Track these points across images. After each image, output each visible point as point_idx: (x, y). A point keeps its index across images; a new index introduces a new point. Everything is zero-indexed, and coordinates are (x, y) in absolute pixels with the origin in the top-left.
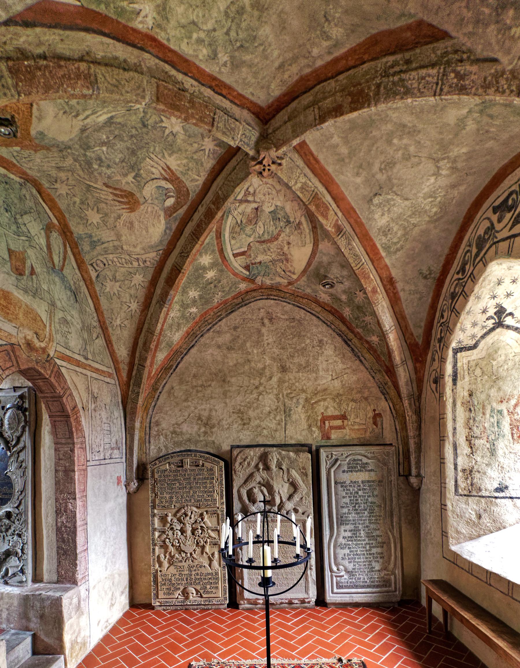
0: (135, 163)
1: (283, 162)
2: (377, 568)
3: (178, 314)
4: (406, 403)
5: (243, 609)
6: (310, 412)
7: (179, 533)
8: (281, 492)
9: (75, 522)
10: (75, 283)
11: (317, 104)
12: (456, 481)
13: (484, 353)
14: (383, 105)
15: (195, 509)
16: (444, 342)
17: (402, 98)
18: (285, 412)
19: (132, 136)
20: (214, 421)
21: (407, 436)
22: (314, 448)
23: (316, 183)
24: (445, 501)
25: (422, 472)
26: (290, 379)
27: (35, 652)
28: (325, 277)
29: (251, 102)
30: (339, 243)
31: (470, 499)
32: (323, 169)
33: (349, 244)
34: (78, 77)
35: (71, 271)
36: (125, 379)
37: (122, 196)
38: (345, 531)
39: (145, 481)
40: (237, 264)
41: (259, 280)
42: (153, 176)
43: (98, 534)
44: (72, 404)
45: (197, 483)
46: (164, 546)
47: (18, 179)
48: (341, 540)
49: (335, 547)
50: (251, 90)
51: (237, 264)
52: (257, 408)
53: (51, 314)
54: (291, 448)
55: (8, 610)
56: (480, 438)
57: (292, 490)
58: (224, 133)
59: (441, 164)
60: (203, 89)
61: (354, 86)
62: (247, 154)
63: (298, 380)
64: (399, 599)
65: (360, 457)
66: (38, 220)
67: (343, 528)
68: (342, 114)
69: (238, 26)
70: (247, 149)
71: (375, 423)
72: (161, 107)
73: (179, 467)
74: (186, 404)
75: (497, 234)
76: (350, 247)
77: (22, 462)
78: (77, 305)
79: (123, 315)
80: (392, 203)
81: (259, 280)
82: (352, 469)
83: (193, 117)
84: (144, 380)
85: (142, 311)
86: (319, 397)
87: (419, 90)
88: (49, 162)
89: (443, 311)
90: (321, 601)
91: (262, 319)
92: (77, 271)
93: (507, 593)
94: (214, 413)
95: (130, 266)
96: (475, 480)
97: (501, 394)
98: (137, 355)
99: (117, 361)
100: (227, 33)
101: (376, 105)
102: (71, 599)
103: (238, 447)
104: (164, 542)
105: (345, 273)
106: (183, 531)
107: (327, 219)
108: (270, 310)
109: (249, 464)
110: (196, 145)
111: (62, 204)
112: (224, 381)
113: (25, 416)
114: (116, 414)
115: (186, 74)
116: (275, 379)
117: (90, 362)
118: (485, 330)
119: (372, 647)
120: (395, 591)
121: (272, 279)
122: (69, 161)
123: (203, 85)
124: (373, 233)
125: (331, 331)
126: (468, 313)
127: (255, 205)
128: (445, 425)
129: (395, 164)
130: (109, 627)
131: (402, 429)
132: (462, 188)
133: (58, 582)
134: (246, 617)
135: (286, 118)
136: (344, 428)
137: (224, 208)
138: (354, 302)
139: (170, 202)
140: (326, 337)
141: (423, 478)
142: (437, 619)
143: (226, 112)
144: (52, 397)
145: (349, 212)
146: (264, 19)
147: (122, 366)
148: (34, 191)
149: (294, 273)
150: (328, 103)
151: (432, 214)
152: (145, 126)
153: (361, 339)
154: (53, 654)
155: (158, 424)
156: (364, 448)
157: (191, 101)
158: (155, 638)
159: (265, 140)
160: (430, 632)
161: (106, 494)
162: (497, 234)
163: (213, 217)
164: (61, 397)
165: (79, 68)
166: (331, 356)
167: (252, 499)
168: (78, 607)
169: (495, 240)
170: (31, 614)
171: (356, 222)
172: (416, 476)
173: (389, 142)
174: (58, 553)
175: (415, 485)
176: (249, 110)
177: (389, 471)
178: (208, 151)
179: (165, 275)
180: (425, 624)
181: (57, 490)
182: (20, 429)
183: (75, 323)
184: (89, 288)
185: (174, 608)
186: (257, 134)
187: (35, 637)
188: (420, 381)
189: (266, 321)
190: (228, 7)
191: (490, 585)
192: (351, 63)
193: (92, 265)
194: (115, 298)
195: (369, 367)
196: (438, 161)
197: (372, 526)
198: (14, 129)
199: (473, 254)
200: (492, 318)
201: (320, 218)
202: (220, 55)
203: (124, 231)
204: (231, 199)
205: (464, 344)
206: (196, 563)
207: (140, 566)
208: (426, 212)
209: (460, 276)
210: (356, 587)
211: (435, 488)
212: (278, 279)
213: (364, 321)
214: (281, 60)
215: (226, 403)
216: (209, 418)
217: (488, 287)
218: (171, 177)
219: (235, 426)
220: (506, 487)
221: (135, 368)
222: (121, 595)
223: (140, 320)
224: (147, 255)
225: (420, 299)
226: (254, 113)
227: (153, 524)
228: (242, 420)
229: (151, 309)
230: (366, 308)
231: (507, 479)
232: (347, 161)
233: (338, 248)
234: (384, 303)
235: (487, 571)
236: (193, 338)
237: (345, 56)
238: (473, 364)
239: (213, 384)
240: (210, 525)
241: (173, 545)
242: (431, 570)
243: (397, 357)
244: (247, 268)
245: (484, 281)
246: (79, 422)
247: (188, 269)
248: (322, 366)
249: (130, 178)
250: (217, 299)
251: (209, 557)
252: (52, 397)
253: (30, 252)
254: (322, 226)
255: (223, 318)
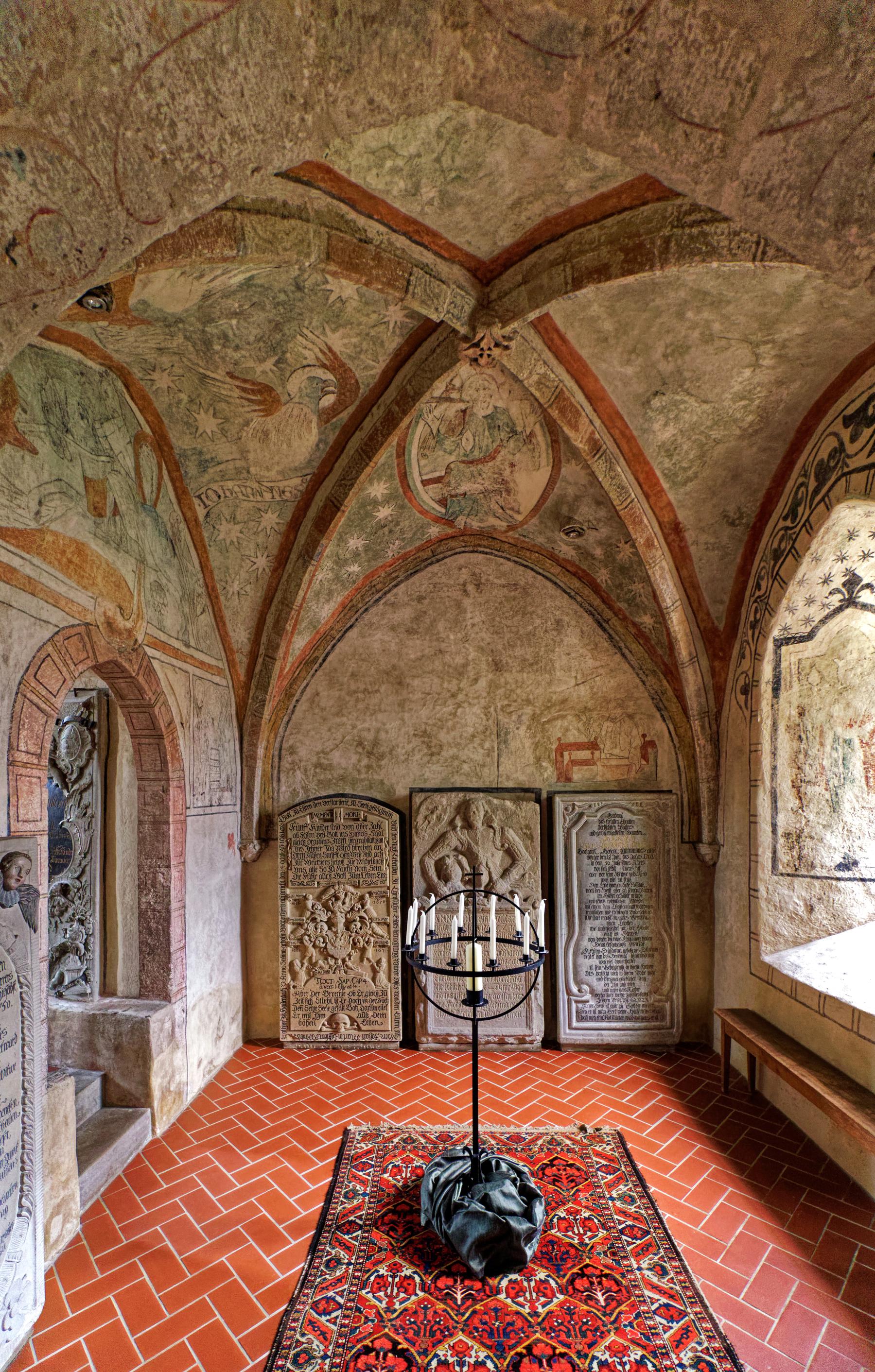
0: (278, 344)
1: (513, 344)
2: (642, 990)
3: (330, 575)
4: (696, 725)
5: (426, 1051)
6: (539, 736)
7: (326, 927)
8: (490, 865)
9: (169, 904)
10: (172, 526)
11: (570, 261)
12: (774, 852)
13: (823, 649)
14: (675, 269)
15: (351, 889)
16: (759, 628)
17: (704, 261)
18: (498, 735)
19: (278, 304)
20: (383, 749)
21: (697, 779)
22: (544, 795)
23: (560, 375)
24: (756, 883)
25: (720, 837)
26: (506, 683)
27: (106, 1102)
28: (570, 519)
29: (467, 254)
30: (595, 467)
31: (797, 881)
32: (572, 352)
33: (611, 469)
34: (218, 233)
35: (168, 508)
36: (242, 678)
37: (253, 392)
38: (593, 929)
39: (272, 843)
40: (428, 497)
41: (461, 522)
42: (305, 363)
43: (201, 924)
44: (167, 719)
45: (355, 848)
46: (300, 947)
47: (97, 367)
48: (585, 944)
49: (575, 954)
50: (468, 237)
51: (428, 497)
52: (453, 728)
53: (140, 576)
54: (507, 795)
55: (63, 1036)
56: (815, 784)
57: (508, 861)
58: (423, 302)
59: (762, 349)
60: (394, 237)
61: (629, 238)
62: (454, 331)
63: (520, 684)
64: (677, 1040)
65: (619, 811)
66: (124, 429)
67: (589, 924)
68: (609, 278)
69: (455, 150)
70: (457, 326)
71: (644, 757)
72: (333, 267)
73: (326, 821)
74: (338, 720)
75: (848, 461)
76: (612, 474)
77: (87, 807)
78: (175, 561)
79: (243, 575)
80: (682, 407)
81: (461, 522)
82: (607, 827)
83: (377, 278)
84: (274, 681)
85: (275, 570)
86: (554, 713)
87: (730, 250)
88: (146, 341)
89: (760, 578)
90: (551, 1042)
91: (464, 585)
92: (176, 507)
93: (849, 1026)
94: (383, 736)
95: (259, 498)
96: (805, 851)
97: (851, 713)
98: (264, 639)
99: (231, 650)
100: (438, 160)
101: (662, 268)
102: (162, 1022)
103: (422, 790)
104: (301, 940)
105: (602, 513)
106: (331, 924)
107: (577, 431)
108: (477, 571)
109: (439, 818)
110: (374, 316)
111: (161, 404)
112: (400, 683)
113: (93, 735)
114: (228, 734)
115: (370, 217)
116: (483, 683)
117: (191, 651)
118: (827, 611)
119: (632, 1111)
120: (672, 1027)
121: (481, 521)
122: (180, 339)
123: (394, 231)
124: (650, 452)
125: (576, 607)
126: (801, 582)
127: (463, 406)
128: (758, 762)
129: (689, 347)
130: (214, 1072)
131: (689, 767)
132: (795, 386)
133: (140, 996)
134: (430, 1063)
135: (519, 278)
136: (594, 764)
137: (414, 413)
138: (614, 560)
139: (328, 400)
140: (568, 614)
141: (721, 846)
142: (737, 1073)
143: (425, 268)
144: (136, 706)
145: (612, 420)
146: (495, 141)
147: (238, 657)
148: (120, 384)
149: (518, 512)
150: (586, 260)
151: (745, 425)
152: (299, 288)
153: (625, 619)
154: (134, 1106)
155: (292, 751)
156: (626, 796)
157: (377, 258)
158: (287, 1089)
159: (485, 310)
160: (727, 1092)
161: (212, 862)
162: (848, 461)
163: (396, 426)
164: (152, 706)
165: (219, 221)
166: (575, 646)
167: (444, 875)
168: (172, 1035)
169: (846, 470)
170: (100, 1043)
171: (622, 433)
172: (710, 844)
173: (680, 315)
174: (141, 952)
175: (707, 858)
176: (462, 265)
177: (665, 834)
178: (392, 320)
179: (313, 513)
180: (719, 1080)
181: (140, 852)
182: (84, 755)
183: (172, 590)
184: (193, 533)
185: (315, 1046)
186: (473, 302)
187: (105, 1079)
188: (719, 690)
189: (470, 588)
190: (442, 125)
191: (824, 1015)
192: (626, 203)
193: (199, 497)
194: (231, 549)
195: (636, 665)
196: (757, 346)
197: (636, 922)
198: (108, 299)
199: (811, 488)
200: (839, 591)
201: (566, 429)
202: (423, 190)
203: (253, 445)
204: (427, 396)
205: (793, 631)
206: (351, 974)
207: (261, 978)
208: (735, 421)
209: (788, 523)
210: (609, 1019)
211: (738, 861)
212: (492, 521)
213: (630, 591)
214: (517, 194)
215: (403, 720)
216: (376, 743)
217: (833, 543)
218: (334, 363)
219: (417, 757)
220: (855, 863)
221: (260, 660)
222: (231, 1023)
223: (269, 586)
224: (286, 483)
225: (722, 558)
226: (469, 270)
227: (284, 912)
228: (429, 747)
229: (289, 567)
230: (634, 570)
231: (857, 850)
232: (612, 341)
233: (592, 474)
234: (664, 563)
235: (820, 994)
236: (351, 613)
237: (618, 192)
238: (806, 664)
239: (383, 688)
240: (375, 915)
241: (314, 946)
242: (732, 993)
243: (683, 651)
244: (443, 502)
245: (826, 533)
246: (176, 747)
247: (351, 504)
248: (560, 661)
249: (269, 365)
250: (393, 550)
251: (372, 967)
252: (136, 706)
253: (113, 480)
254: (567, 440)
255: (401, 582)
